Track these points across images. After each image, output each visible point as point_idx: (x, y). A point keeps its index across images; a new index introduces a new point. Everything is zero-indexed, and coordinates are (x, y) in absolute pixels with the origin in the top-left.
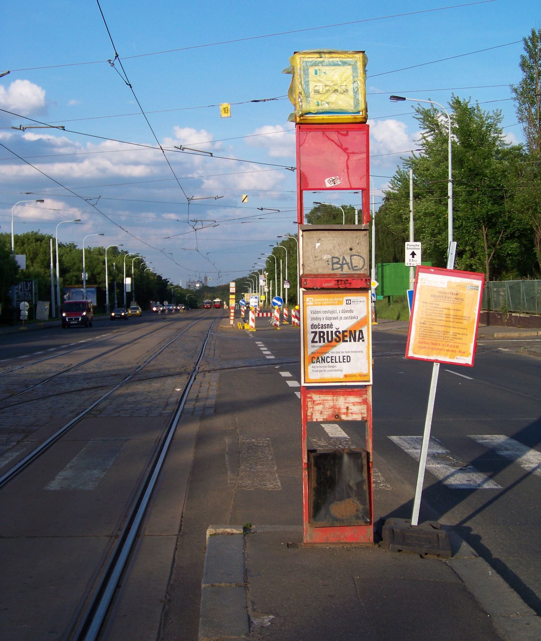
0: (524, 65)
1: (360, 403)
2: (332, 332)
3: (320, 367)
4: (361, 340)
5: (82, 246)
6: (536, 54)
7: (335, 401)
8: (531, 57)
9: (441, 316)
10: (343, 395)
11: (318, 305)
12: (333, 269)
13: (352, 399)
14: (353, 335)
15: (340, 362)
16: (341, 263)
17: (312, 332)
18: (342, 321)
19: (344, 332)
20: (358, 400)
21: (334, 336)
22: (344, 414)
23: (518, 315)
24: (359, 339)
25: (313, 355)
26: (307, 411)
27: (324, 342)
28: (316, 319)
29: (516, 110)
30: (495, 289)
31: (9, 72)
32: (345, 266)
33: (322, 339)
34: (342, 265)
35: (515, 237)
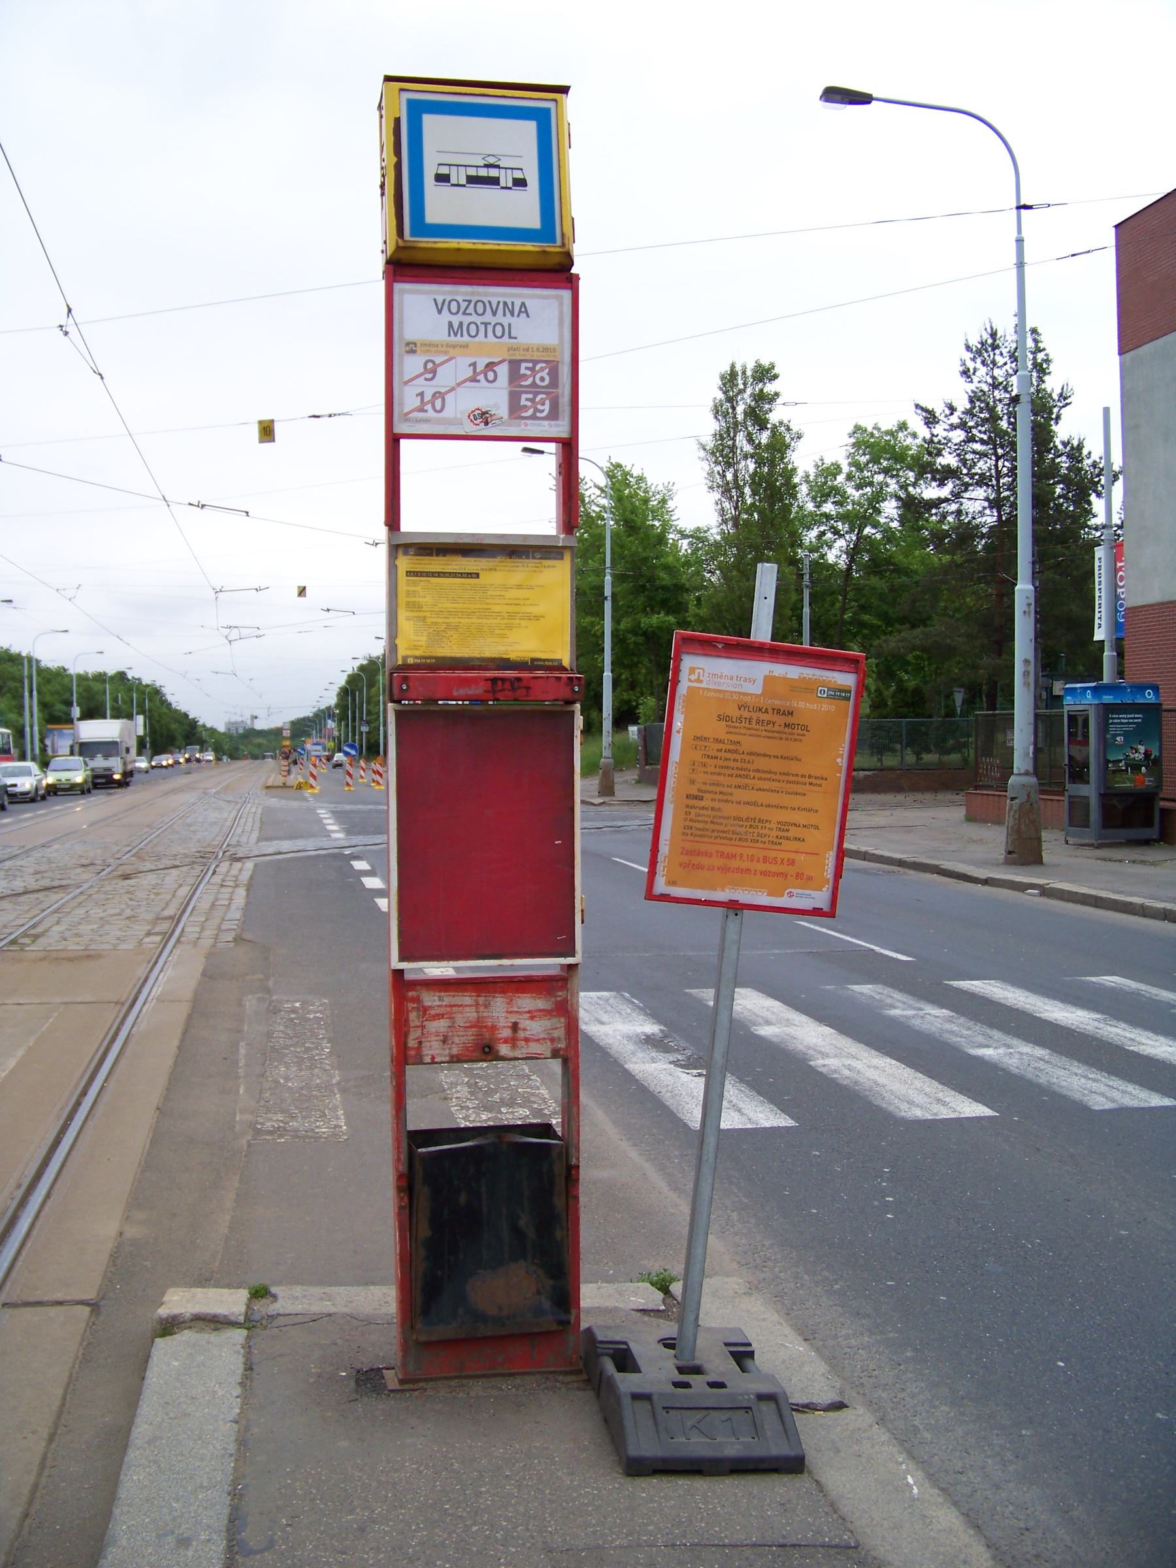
1: (547, 1013)
5: (72, 671)
7: (482, 1009)
9: (747, 777)
13: (527, 1002)
20: (541, 1003)
22: (506, 1041)
26: (406, 1035)
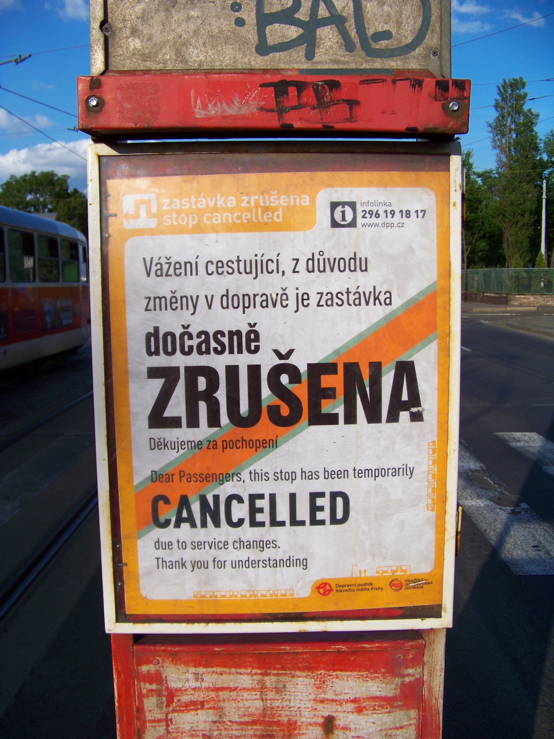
0: (496, 107)
1: (387, 703)
2: (254, 371)
3: (197, 545)
4: (404, 415)
6: (507, 97)
7: (271, 695)
8: (503, 100)
10: (310, 669)
11: (182, 230)
12: (263, 48)
13: (351, 685)
14: (358, 387)
15: (295, 522)
16: (303, 14)
17: (153, 373)
18: (310, 313)
19: (317, 370)
21: (266, 392)
23: (489, 295)
24: (397, 406)
25: (161, 489)
27: (214, 421)
28: (175, 302)
29: (490, 140)
30: (471, 276)
31: (30, 56)
32: (328, 36)
33: (203, 406)
34: (310, 28)
35: (486, 237)
